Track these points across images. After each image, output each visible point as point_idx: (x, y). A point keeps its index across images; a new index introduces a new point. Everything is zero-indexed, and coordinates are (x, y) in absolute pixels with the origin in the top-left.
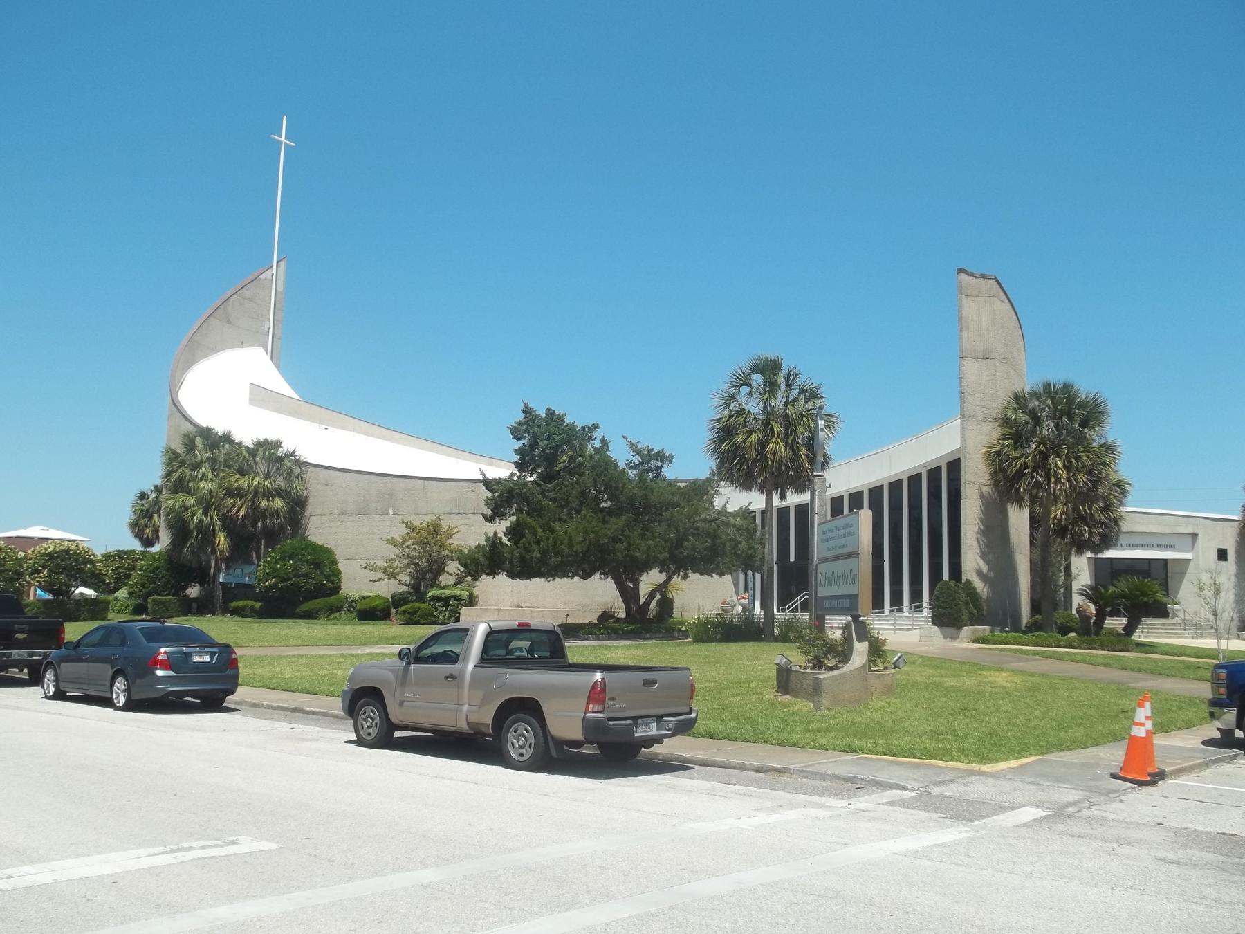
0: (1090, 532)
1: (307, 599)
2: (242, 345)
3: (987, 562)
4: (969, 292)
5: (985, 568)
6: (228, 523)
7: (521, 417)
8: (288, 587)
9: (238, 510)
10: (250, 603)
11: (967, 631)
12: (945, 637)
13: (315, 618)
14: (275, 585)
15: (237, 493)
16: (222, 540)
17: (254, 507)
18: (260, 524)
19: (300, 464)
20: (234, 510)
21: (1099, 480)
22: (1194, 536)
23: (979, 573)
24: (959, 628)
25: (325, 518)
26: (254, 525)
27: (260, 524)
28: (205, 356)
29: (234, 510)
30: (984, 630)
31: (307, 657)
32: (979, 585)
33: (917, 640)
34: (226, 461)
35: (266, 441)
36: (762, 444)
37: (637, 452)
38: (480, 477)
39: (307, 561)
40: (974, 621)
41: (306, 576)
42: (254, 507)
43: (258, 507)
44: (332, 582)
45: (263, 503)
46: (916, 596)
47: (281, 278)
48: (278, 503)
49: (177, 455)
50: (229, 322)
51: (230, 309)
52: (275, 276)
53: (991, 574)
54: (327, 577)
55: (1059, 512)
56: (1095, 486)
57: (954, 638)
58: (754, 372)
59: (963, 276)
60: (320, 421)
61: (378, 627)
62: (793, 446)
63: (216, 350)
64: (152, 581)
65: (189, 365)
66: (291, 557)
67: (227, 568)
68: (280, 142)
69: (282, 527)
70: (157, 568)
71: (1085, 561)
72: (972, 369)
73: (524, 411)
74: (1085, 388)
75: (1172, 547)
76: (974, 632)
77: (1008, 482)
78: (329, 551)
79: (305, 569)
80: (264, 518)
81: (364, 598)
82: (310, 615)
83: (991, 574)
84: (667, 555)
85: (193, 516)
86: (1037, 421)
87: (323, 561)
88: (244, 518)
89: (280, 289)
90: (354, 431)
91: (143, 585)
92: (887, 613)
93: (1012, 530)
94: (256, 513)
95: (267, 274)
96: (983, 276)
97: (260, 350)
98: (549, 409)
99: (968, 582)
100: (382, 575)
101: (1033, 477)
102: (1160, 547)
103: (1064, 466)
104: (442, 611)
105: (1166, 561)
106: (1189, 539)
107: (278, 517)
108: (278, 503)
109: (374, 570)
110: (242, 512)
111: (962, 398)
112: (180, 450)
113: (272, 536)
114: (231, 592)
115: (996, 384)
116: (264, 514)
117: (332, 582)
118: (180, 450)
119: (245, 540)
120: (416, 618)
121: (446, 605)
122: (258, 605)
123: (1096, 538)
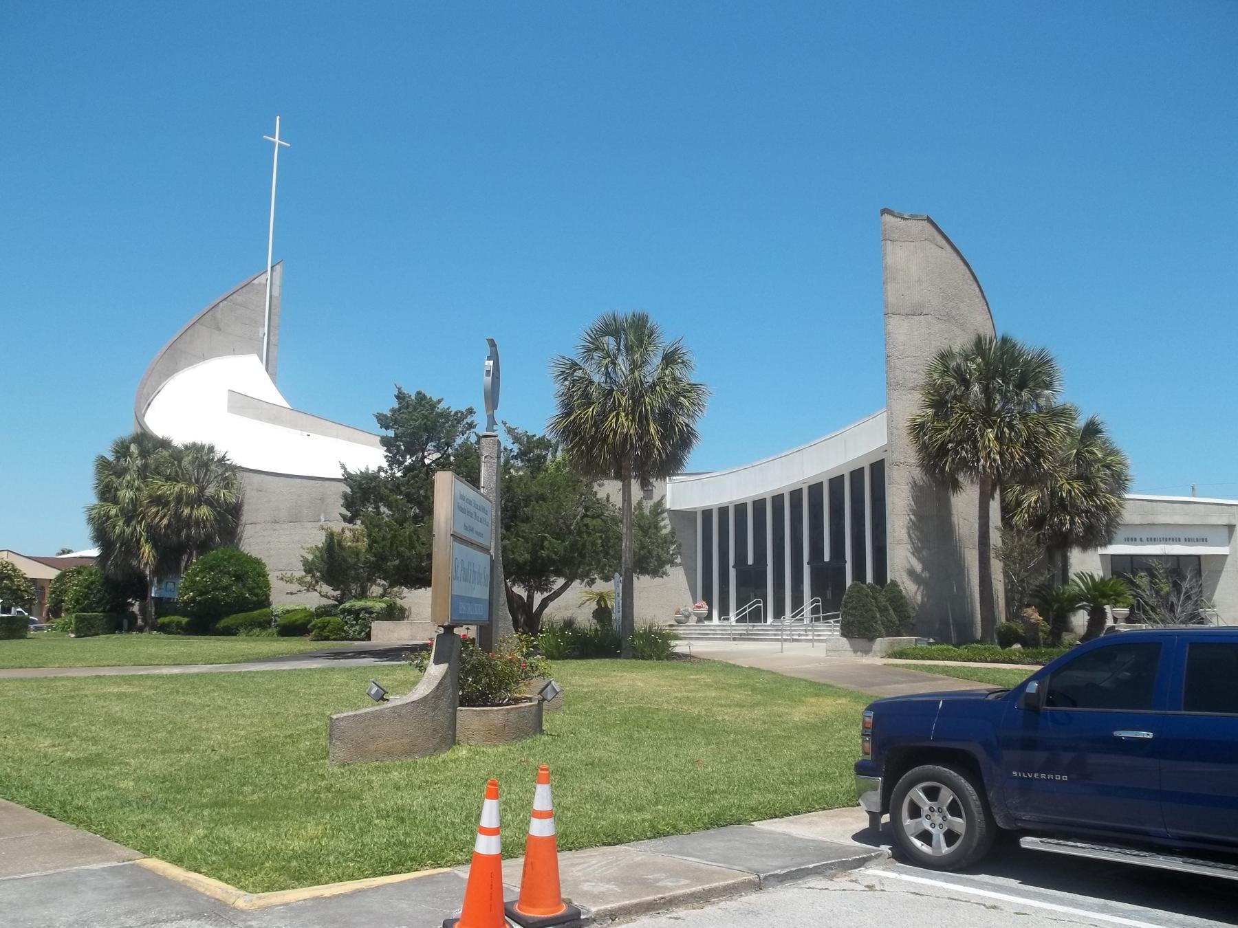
0: (1072, 522)
1: (228, 614)
2: (234, 352)
3: (919, 559)
4: (895, 236)
5: (918, 567)
6: (154, 536)
7: (395, 404)
8: (206, 600)
9: (161, 519)
10: (176, 618)
11: (881, 643)
12: (855, 651)
13: (235, 634)
14: (193, 600)
15: (159, 501)
16: (146, 549)
17: (177, 516)
18: (183, 534)
19: (235, 469)
20: (157, 519)
21: (1040, 454)
22: (1231, 527)
23: (911, 573)
24: (872, 639)
25: (259, 526)
26: (180, 536)
27: (183, 534)
28: (190, 364)
29: (157, 519)
30: (907, 641)
31: (74, 679)
32: (909, 588)
33: (823, 654)
34: (157, 467)
35: (194, 444)
36: (604, 415)
37: (517, 439)
38: (339, 474)
39: (229, 573)
40: (893, 630)
41: (225, 589)
42: (177, 516)
43: (181, 515)
44: (256, 595)
45: (187, 511)
46: (798, 602)
47: (277, 282)
48: (204, 511)
49: (109, 463)
50: (219, 329)
51: (219, 316)
52: (270, 281)
53: (926, 575)
54: (251, 590)
55: (1033, 499)
56: (1036, 461)
57: (866, 652)
58: (606, 333)
59: (887, 217)
60: (301, 428)
61: (219, 643)
62: (642, 422)
63: (204, 358)
64: (86, 597)
65: (169, 371)
66: (211, 569)
67: (159, 582)
68: (274, 143)
69: (210, 537)
70: (92, 583)
71: (1098, 559)
72: (901, 329)
73: (397, 397)
74: (1029, 341)
75: (1204, 541)
76: (892, 645)
77: (941, 460)
78: (258, 562)
79: (226, 581)
80: (189, 526)
81: (288, 611)
82: (229, 632)
83: (926, 575)
84: (527, 556)
85: (114, 527)
86: (967, 384)
87: (251, 576)
88: (168, 526)
89: (276, 293)
90: (337, 437)
91: (77, 602)
92: (806, 621)
93: (955, 519)
94: (180, 523)
95: (261, 279)
96: (913, 217)
97: (254, 358)
98: (419, 393)
99: (894, 584)
100: (299, 587)
101: (957, 453)
102: (1189, 541)
103: (996, 438)
104: (352, 625)
105: (1199, 557)
106: (1225, 532)
107: (205, 527)
108: (204, 511)
109: (290, 581)
110: (165, 521)
111: (887, 362)
112: (111, 457)
113: (204, 546)
114: (164, 606)
115: (917, 345)
116: (188, 523)
117: (256, 595)
118: (111, 457)
119: (171, 555)
120: (326, 633)
121: (357, 619)
122: (185, 620)
123: (1080, 530)
